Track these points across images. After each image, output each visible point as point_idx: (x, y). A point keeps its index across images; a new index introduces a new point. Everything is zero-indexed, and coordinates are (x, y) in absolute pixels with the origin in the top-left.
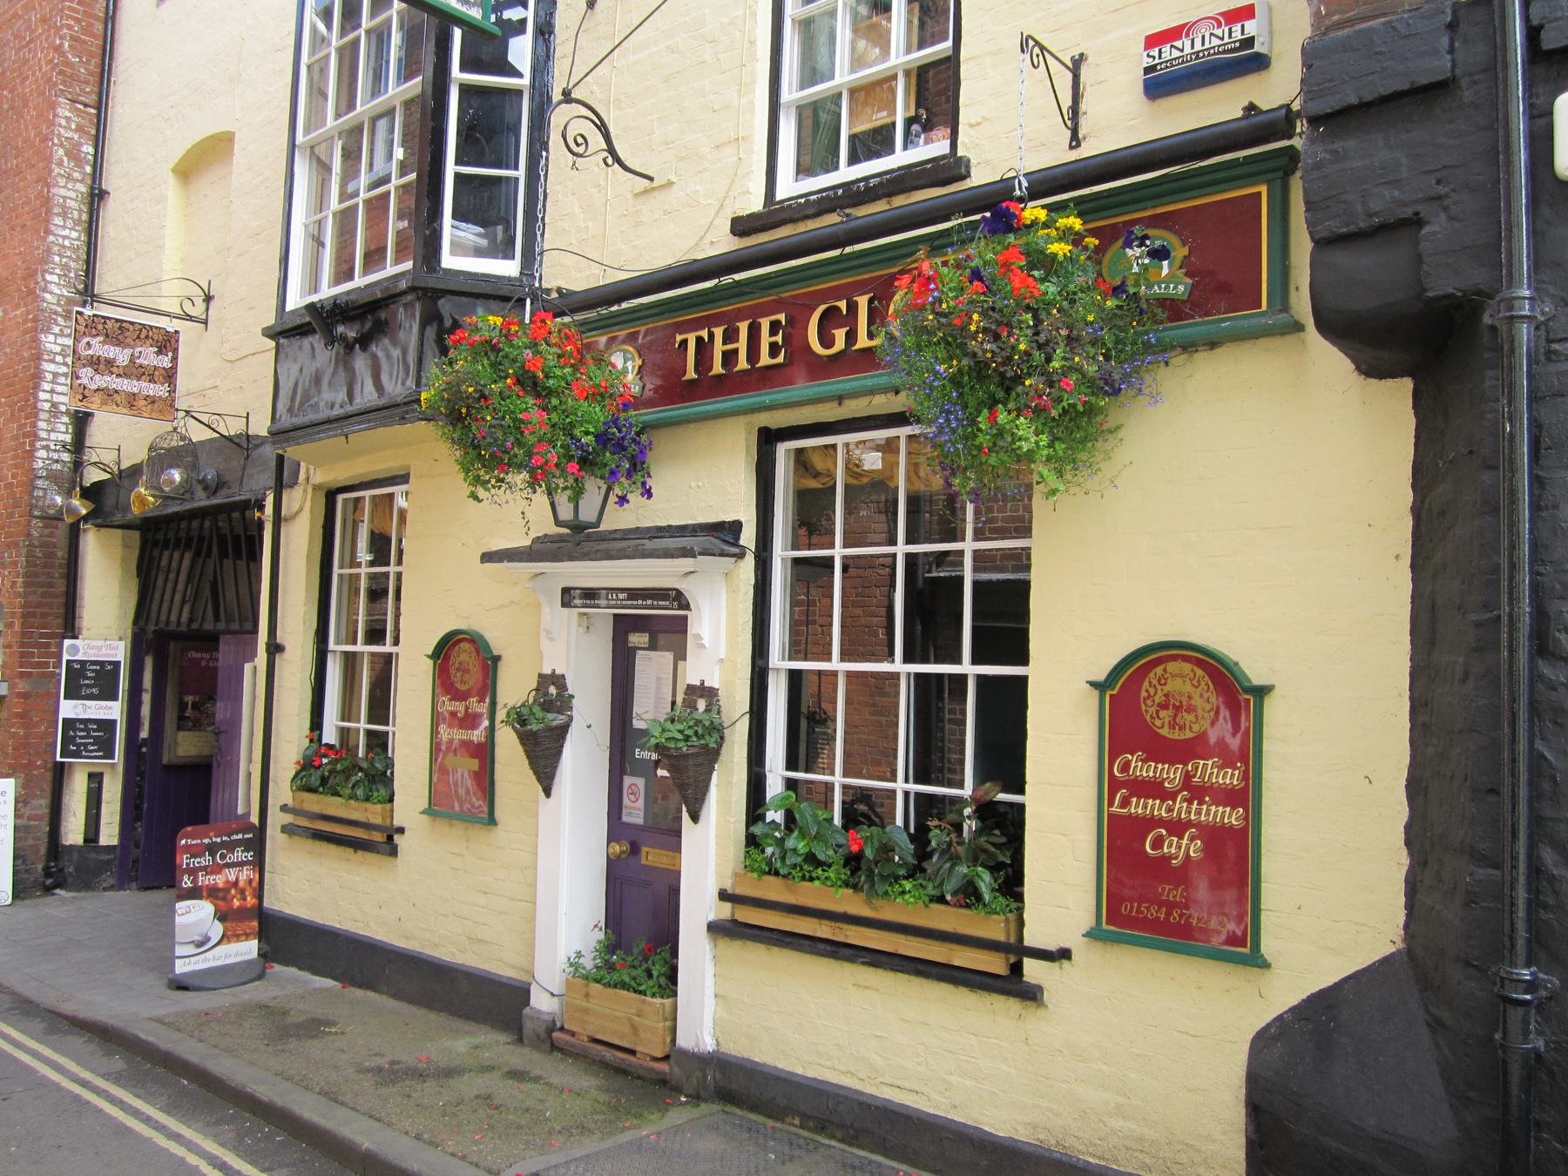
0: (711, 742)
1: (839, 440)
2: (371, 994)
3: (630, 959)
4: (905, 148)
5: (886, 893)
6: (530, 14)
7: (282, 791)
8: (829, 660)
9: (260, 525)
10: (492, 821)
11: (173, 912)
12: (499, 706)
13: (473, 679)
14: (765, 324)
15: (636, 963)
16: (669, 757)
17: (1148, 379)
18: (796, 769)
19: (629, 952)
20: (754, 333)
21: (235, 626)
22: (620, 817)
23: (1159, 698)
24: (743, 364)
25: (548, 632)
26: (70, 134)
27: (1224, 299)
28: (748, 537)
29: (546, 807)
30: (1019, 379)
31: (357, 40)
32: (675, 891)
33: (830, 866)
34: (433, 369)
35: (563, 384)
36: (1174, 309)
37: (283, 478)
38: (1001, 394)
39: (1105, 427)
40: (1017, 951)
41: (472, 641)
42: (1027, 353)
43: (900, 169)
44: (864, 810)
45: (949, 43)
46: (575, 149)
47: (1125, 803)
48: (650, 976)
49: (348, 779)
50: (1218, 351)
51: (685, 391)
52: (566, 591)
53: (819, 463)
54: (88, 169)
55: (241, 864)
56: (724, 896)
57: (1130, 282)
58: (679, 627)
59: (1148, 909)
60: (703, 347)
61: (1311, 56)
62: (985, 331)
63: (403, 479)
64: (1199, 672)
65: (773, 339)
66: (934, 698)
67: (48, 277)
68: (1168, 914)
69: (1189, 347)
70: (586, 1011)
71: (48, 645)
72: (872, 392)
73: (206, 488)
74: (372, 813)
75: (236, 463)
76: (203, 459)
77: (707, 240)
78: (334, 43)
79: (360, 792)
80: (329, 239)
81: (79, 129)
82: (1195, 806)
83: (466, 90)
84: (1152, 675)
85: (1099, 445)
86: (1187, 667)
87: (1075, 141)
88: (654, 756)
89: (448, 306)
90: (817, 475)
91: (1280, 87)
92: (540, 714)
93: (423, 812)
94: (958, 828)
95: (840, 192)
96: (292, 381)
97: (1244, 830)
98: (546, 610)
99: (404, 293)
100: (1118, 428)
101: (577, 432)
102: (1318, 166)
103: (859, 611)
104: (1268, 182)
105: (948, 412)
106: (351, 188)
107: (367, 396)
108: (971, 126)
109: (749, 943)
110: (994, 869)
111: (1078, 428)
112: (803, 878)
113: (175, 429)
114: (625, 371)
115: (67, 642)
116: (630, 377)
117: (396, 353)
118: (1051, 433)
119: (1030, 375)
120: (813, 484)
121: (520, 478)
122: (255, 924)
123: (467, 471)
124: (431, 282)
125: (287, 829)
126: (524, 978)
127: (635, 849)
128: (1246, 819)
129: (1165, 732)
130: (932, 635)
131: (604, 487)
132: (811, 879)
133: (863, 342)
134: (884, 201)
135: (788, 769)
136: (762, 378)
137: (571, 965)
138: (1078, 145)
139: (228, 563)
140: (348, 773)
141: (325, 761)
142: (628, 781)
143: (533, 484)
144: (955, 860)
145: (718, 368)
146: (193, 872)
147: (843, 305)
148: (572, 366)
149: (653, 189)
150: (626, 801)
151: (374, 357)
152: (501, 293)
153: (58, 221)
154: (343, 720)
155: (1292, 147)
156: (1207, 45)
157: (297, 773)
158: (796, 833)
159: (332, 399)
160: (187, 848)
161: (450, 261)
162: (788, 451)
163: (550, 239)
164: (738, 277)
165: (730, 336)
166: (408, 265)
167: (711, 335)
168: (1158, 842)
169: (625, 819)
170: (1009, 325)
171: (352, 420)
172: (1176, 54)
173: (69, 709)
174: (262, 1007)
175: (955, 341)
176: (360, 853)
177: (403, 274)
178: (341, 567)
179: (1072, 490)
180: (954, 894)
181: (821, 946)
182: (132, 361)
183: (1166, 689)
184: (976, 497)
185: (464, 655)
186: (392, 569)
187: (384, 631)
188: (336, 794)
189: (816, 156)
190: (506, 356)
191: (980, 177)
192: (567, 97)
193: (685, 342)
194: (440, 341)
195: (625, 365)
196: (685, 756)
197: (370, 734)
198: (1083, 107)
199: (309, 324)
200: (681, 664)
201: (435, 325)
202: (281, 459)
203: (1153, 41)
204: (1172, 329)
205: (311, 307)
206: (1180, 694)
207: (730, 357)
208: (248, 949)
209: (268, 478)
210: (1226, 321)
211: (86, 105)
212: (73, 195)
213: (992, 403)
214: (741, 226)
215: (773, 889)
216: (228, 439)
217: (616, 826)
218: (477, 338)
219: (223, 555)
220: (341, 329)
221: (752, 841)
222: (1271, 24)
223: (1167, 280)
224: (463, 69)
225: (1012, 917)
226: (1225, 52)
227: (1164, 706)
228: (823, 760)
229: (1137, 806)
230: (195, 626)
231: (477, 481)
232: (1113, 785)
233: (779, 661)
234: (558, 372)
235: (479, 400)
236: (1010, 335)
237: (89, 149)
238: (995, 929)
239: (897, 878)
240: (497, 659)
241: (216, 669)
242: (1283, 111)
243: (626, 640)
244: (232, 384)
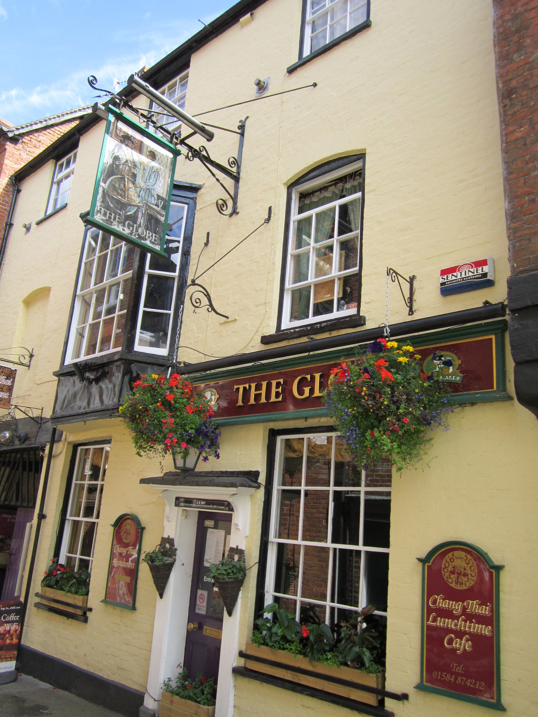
0: (240, 576)
1: (305, 436)
2: (66, 693)
3: (194, 684)
4: (338, 310)
5: (319, 659)
6: (181, 245)
7: (37, 586)
8: (297, 539)
9: (42, 458)
10: (134, 608)
12: (142, 552)
13: (131, 538)
14: (274, 383)
15: (197, 686)
16: (219, 583)
17: (444, 419)
18: (279, 592)
19: (194, 680)
20: (269, 386)
21: (25, 504)
22: (194, 610)
23: (450, 568)
24: (263, 400)
25: (168, 517)
27: (475, 385)
28: (262, 479)
29: (160, 603)
30: (384, 417)
31: (107, 254)
32: (218, 649)
33: (293, 643)
34: (127, 396)
35: (182, 406)
36: (454, 387)
37: (55, 438)
38: (376, 423)
39: (425, 439)
40: (382, 693)
41: (132, 519)
42: (388, 405)
43: (335, 319)
44: (310, 614)
45: (357, 268)
46: (196, 305)
47: (435, 620)
48: (203, 694)
49: (68, 582)
50: (475, 407)
51: (238, 411)
52: (177, 499)
53: (296, 446)
55: (12, 622)
56: (241, 654)
57: (436, 374)
58: (228, 519)
59: (446, 675)
60: (246, 392)
61: (511, 283)
62: (369, 395)
63: (108, 441)
64: (469, 557)
65: (277, 390)
66: (347, 560)
68: (456, 679)
69: (462, 404)
70: (170, 710)
72: (320, 416)
73: (20, 440)
74: (77, 600)
75: (35, 429)
76: (20, 426)
77: (250, 345)
78: (97, 254)
79: (73, 589)
80: (86, 334)
82: (468, 624)
83: (151, 277)
84: (447, 557)
85: (422, 446)
86: (463, 554)
87: (411, 312)
88: (213, 581)
89: (135, 368)
90: (294, 451)
91: (498, 294)
92: (160, 558)
93: (102, 601)
94: (355, 627)
95: (309, 328)
96: (64, 395)
97: (492, 637)
98: (167, 508)
99: (116, 361)
100: (431, 439)
101: (187, 428)
102: (516, 330)
103: (314, 511)
104: (496, 334)
105: (352, 430)
106: (99, 309)
107: (96, 404)
108: (366, 303)
109: (252, 680)
110: (371, 649)
111: (412, 439)
112: (280, 648)
113: (9, 413)
114: (211, 400)
116: (213, 403)
117: (110, 386)
118: (399, 441)
119: (389, 415)
120: (293, 455)
121: (160, 447)
122: (16, 652)
123: (137, 443)
124: (129, 357)
125: (37, 605)
126: (141, 690)
127: (200, 627)
128: (492, 632)
129: (453, 585)
130: (344, 531)
131: (198, 452)
132: (284, 649)
133: (317, 393)
134: (328, 333)
135: (275, 591)
136: (270, 407)
137: (165, 685)
138: (412, 314)
139: (25, 473)
140: (69, 579)
141: (59, 572)
142: (200, 592)
143: (166, 450)
144: (354, 644)
145: (252, 401)
147: (308, 377)
148: (187, 398)
149: (228, 322)
150: (198, 602)
151: (101, 388)
152: (159, 363)
154: (69, 553)
155: (505, 320)
156: (467, 275)
157: (45, 578)
158: (277, 625)
159: (81, 404)
161: (138, 348)
162: (282, 440)
163: (183, 341)
165: (258, 387)
166: (119, 349)
167: (250, 387)
168: (450, 642)
169: (197, 611)
170: (380, 393)
171: (89, 415)
172: (454, 278)
174: (14, 697)
175: (356, 398)
176: (70, 619)
177: (117, 352)
178: (77, 480)
179: (410, 467)
180: (352, 662)
181: (287, 684)
183: (454, 564)
184: (366, 467)
185: (129, 526)
186: (99, 483)
187: (94, 507)
188: (62, 589)
189: (299, 312)
190: (158, 393)
191: (370, 325)
192: (193, 283)
193: (238, 389)
194: (130, 383)
195: (211, 398)
196: (227, 583)
197: (81, 560)
198: (415, 298)
199: (73, 371)
200: (228, 536)
201: (129, 376)
202: (54, 430)
203: (444, 272)
204: (453, 396)
205: (75, 365)
206: (460, 567)
207: (258, 397)
209: (48, 437)
210: (478, 393)
213: (372, 427)
214: (266, 340)
215: (265, 653)
216: (32, 418)
217: (193, 616)
218: (146, 384)
219: (24, 469)
220: (87, 374)
221: (256, 627)
222: (494, 268)
223: (452, 374)
224: (150, 268)
225: (380, 675)
226: (473, 279)
227: (453, 573)
228: (292, 588)
229: (440, 622)
230: (7, 503)
231: (141, 447)
232: (429, 610)
233: (273, 539)
234: (181, 401)
235: (144, 412)
236: (380, 397)
238: (371, 681)
239: (325, 651)
240: (143, 529)
241: (14, 523)
242: (500, 305)
243: (203, 523)
244: (36, 395)
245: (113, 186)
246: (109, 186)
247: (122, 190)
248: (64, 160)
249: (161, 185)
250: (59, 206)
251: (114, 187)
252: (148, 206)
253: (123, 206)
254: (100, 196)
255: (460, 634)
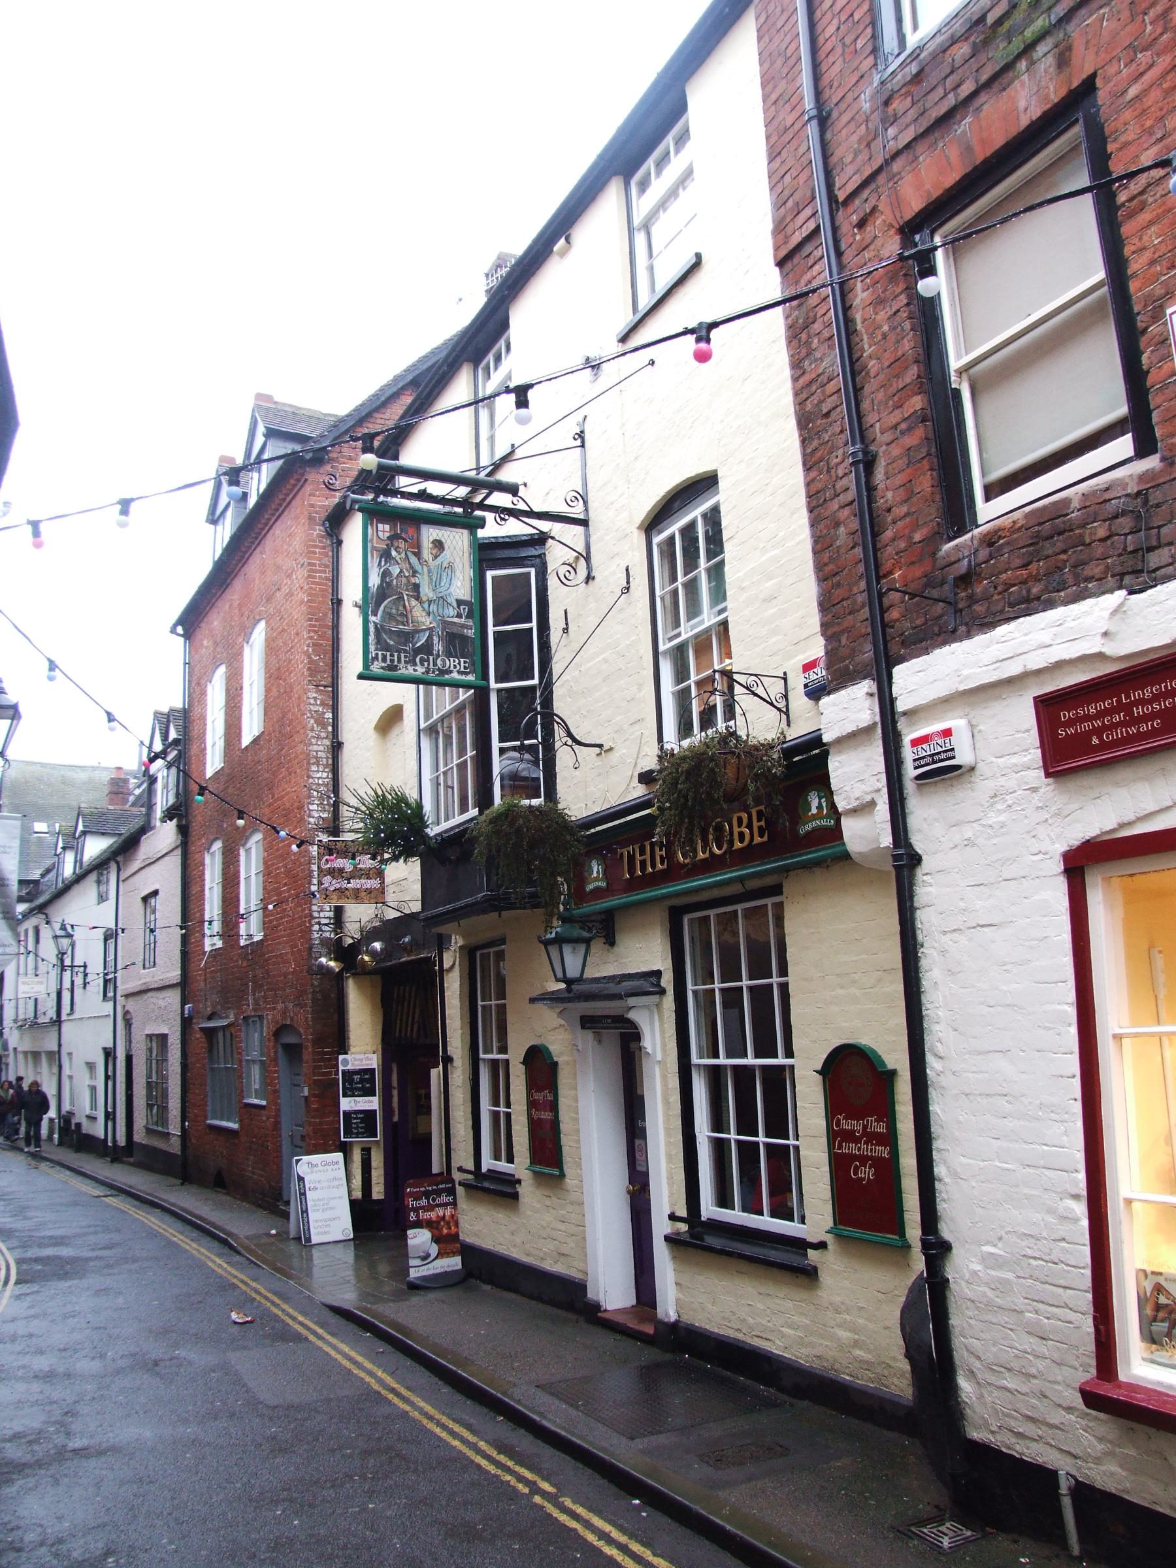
11: (405, 1238)
26: (317, 708)
28: (667, 981)
54: (330, 729)
63: (503, 941)
67: (311, 807)
71: (329, 1060)
81: (323, 704)
115: (341, 1057)
146: (416, 1210)
153: (314, 768)
160: (411, 1194)
164: (598, 829)
173: (346, 1104)
182: (355, 867)
186: (775, 980)
193: (622, 854)
208: (454, 1263)
211: (325, 687)
212: (322, 748)
237: (329, 715)
245: (388, 616)
246: (382, 617)
247: (402, 615)
248: (490, 357)
249: (459, 584)
250: (499, 455)
251: (390, 614)
252: (445, 622)
253: (407, 637)
254: (372, 637)
255: (863, 1160)
